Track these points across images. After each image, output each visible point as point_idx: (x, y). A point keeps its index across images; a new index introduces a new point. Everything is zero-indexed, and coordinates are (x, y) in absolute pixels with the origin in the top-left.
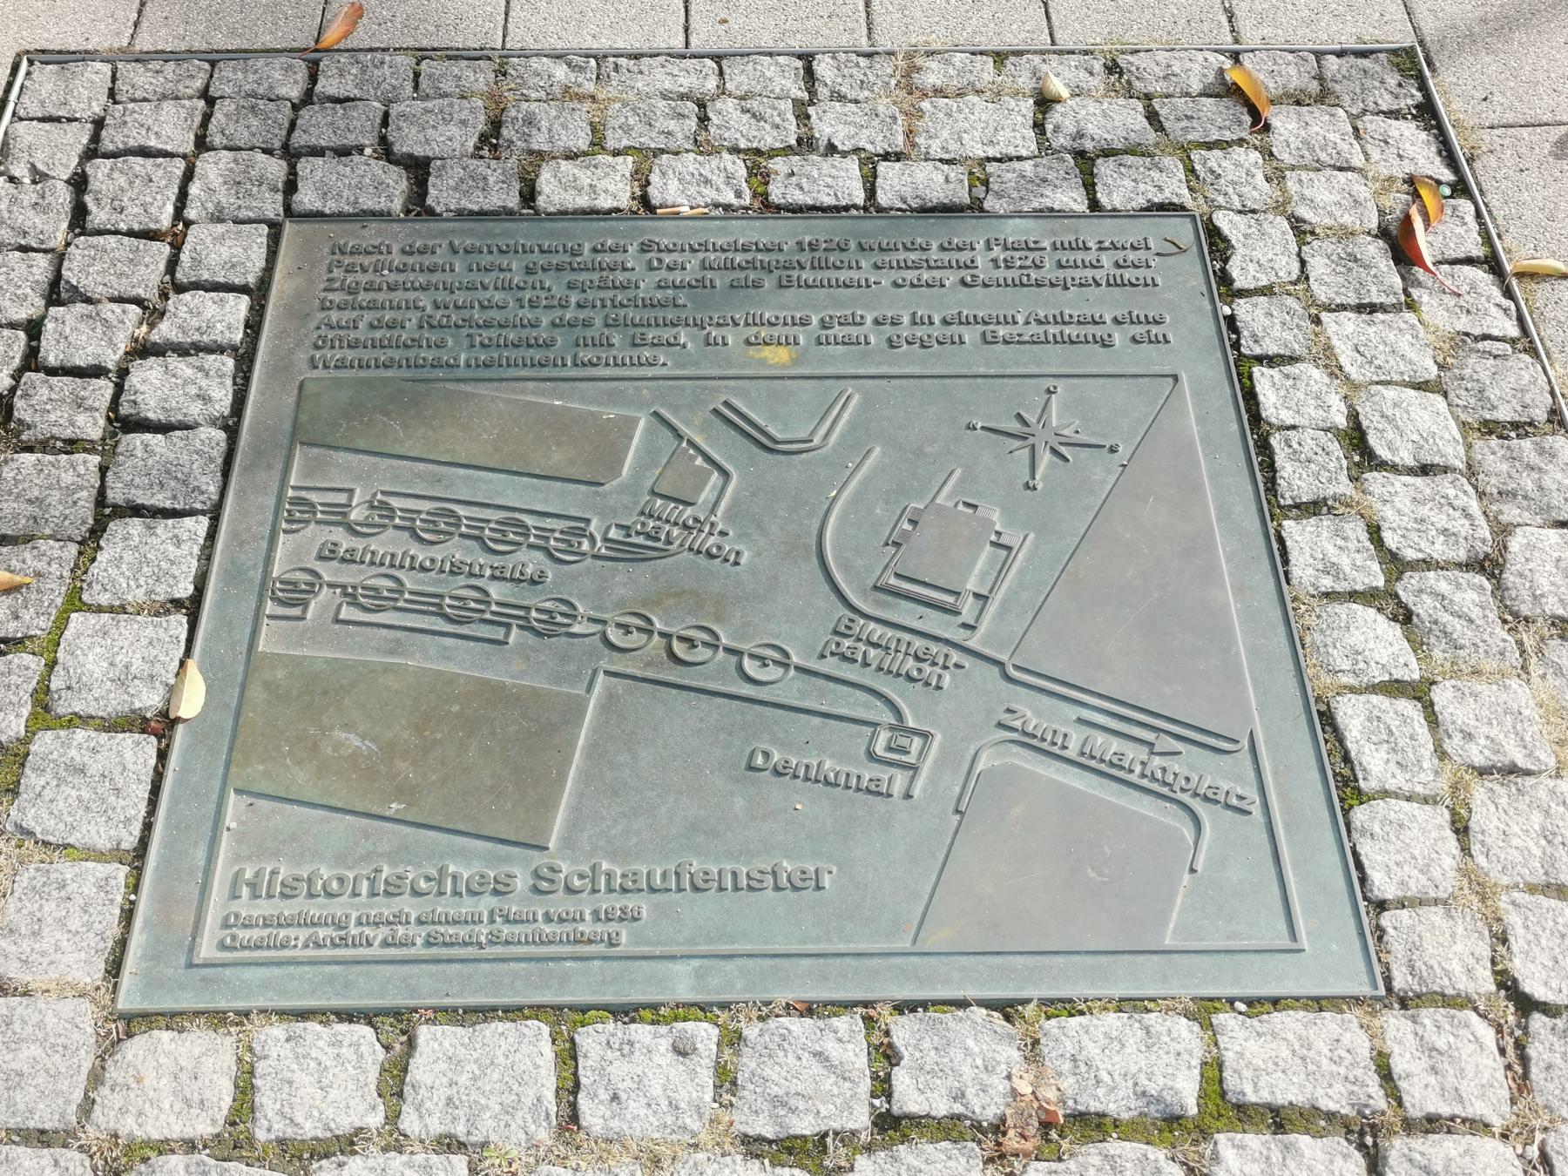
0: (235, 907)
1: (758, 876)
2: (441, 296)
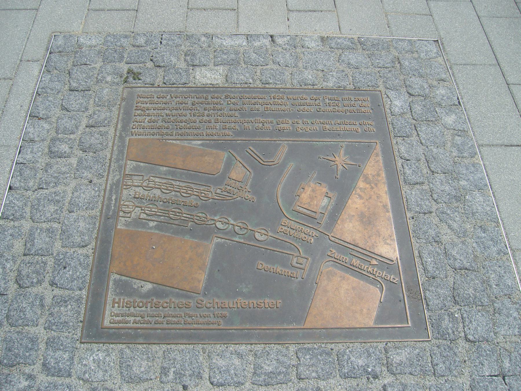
0: (113, 310)
1: (260, 304)
2: (167, 112)
